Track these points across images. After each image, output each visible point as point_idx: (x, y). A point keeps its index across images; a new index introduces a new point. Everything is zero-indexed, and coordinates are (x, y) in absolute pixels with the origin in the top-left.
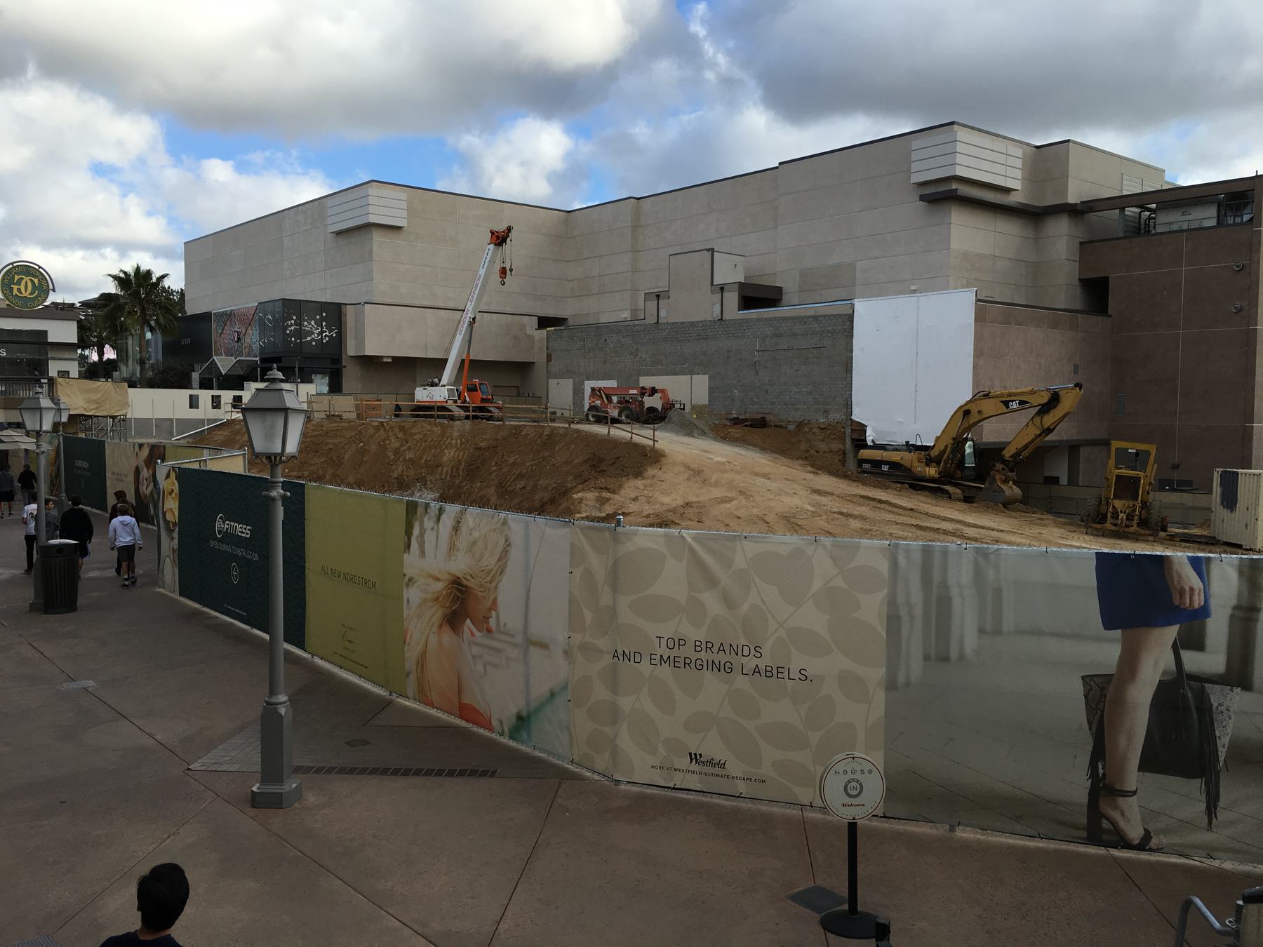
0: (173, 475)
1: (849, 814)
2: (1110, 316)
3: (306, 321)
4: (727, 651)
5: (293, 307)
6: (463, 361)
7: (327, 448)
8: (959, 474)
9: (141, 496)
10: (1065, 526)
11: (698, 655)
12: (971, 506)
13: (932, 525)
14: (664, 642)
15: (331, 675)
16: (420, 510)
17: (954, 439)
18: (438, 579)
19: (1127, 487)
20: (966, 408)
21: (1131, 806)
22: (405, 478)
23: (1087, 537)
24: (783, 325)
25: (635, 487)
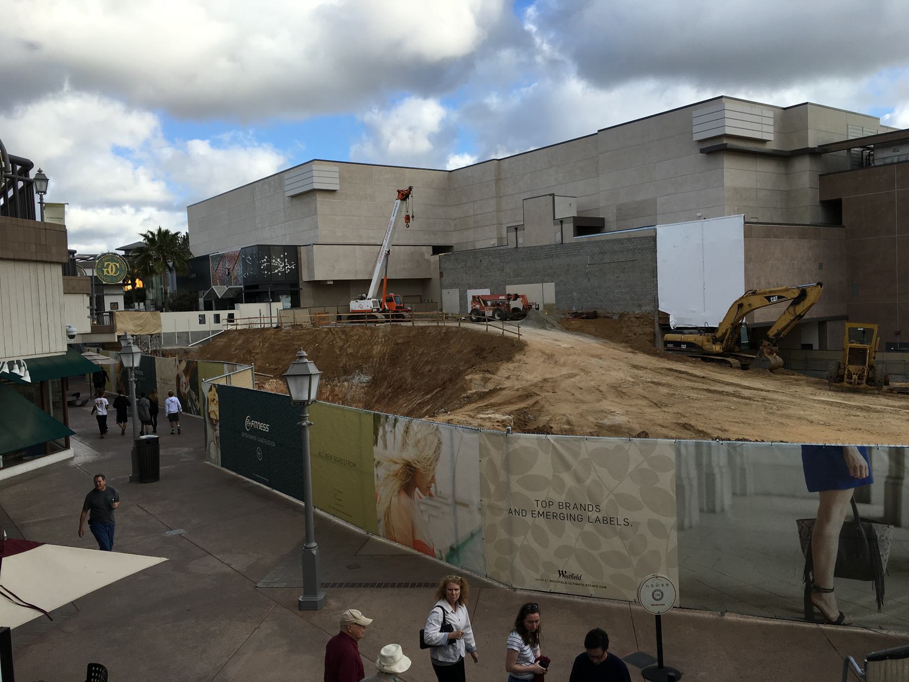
0: (214, 389)
1: (655, 610)
2: (844, 227)
3: (274, 259)
4: (579, 508)
5: (265, 250)
6: (382, 280)
7: (294, 348)
8: (737, 349)
9: (181, 395)
11: (561, 511)
12: (746, 372)
14: (540, 503)
15: (329, 521)
16: (382, 420)
17: (732, 324)
18: (396, 463)
19: (858, 356)
20: (740, 302)
21: (831, 598)
22: (348, 366)
23: (830, 393)
25: (508, 369)
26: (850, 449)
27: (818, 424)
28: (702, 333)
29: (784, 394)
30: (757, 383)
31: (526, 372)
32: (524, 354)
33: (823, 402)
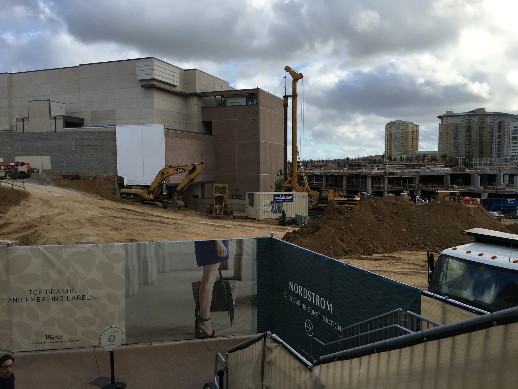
1: (110, 349)
2: (213, 135)
4: (61, 292)
10: (199, 216)
11: (48, 296)
12: (166, 210)
13: (151, 219)
14: (32, 292)
17: (158, 184)
19: (219, 200)
21: (208, 323)
23: (207, 220)
24: (85, 135)
26: (218, 242)
27: (201, 236)
28: (142, 188)
29: (185, 221)
30: (171, 215)
31: (29, 212)
32: (28, 201)
33: (204, 224)
